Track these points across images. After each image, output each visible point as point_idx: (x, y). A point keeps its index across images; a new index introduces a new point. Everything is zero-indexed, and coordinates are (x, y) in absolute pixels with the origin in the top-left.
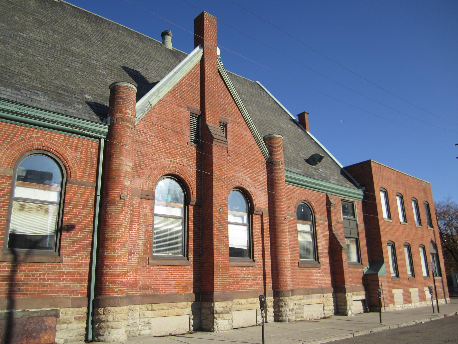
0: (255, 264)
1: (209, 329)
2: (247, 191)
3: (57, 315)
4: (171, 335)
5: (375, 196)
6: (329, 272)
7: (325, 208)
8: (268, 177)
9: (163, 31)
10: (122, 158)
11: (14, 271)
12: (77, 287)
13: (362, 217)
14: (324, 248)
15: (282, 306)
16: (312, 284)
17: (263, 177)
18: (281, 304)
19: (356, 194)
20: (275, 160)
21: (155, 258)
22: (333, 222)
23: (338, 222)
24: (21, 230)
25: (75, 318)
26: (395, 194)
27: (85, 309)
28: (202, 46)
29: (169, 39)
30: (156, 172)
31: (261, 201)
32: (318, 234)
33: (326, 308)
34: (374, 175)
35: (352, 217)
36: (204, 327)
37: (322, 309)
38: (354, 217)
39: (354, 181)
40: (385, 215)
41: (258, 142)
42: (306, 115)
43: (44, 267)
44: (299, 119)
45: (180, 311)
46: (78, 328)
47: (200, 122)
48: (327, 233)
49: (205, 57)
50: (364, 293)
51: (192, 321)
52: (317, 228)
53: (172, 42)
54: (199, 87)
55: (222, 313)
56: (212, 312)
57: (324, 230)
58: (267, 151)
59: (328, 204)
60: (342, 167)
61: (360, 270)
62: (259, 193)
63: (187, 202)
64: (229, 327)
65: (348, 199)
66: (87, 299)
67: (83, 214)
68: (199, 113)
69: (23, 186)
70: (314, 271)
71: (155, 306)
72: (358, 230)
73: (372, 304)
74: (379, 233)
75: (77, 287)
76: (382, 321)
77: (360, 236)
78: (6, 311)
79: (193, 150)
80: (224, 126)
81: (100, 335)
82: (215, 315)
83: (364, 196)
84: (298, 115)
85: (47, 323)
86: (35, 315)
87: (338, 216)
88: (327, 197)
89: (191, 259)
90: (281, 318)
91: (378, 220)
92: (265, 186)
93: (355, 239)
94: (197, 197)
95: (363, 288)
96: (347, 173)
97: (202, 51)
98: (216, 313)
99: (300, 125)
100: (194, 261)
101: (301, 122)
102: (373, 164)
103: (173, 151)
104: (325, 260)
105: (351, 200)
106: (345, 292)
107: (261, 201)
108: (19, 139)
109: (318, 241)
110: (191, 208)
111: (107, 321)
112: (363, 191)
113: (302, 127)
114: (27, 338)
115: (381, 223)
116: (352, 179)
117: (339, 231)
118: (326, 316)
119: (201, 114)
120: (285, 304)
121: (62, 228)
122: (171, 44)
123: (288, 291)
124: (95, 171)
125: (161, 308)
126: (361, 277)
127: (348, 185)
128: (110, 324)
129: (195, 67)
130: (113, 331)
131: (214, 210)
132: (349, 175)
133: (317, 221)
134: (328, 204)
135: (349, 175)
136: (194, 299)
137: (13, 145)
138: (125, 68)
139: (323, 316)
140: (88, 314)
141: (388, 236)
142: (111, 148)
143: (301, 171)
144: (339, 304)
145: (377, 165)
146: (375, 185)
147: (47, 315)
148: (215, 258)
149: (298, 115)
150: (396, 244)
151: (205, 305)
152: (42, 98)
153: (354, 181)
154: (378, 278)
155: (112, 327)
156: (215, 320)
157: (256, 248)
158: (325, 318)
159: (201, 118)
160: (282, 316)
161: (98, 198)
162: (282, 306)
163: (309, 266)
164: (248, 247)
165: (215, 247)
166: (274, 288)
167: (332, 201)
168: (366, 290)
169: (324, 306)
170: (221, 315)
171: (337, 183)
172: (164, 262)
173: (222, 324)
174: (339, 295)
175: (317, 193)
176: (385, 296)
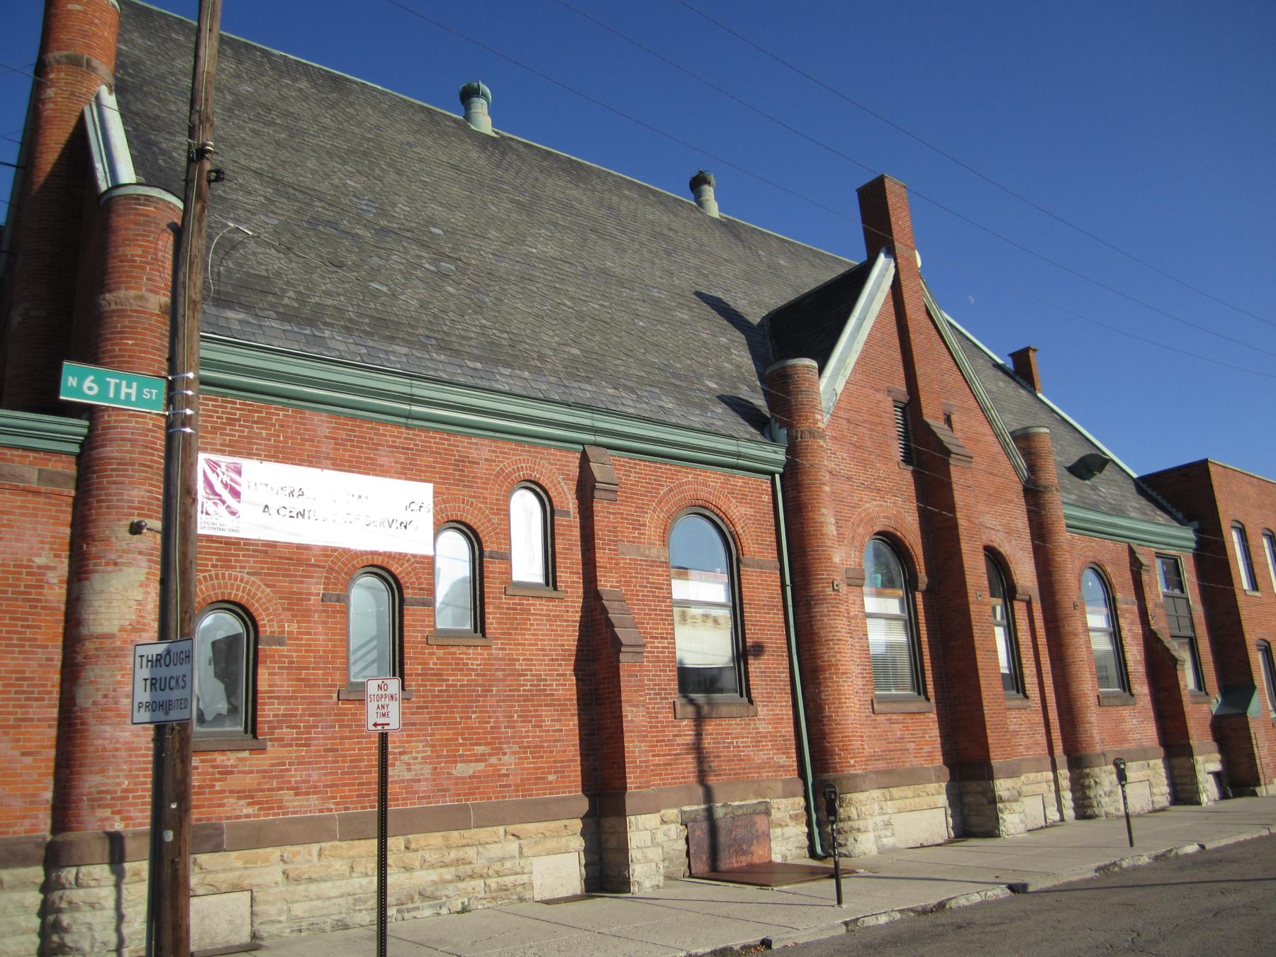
0: (1030, 703)
1: (990, 830)
2: (1000, 553)
3: (767, 813)
4: (922, 846)
5: (1223, 542)
6: (1152, 714)
7: (1128, 575)
8: (1030, 520)
9: (695, 174)
10: (824, 510)
11: (699, 735)
12: (782, 759)
13: (1197, 591)
14: (1136, 662)
15: (1089, 787)
16: (1125, 740)
17: (1021, 522)
18: (1087, 782)
19: (1181, 538)
20: (1042, 482)
21: (882, 700)
22: (1150, 605)
23: (1156, 605)
24: (691, 661)
25: (791, 816)
26: (1260, 531)
27: (801, 801)
28: (891, 252)
29: (709, 192)
30: (861, 530)
31: (1025, 573)
32: (1124, 633)
33: (1155, 790)
34: (1217, 494)
35: (1177, 592)
36: (974, 829)
37: (1147, 791)
38: (1182, 591)
39: (1169, 507)
40: (1245, 584)
41: (1004, 447)
42: (1031, 354)
43: (735, 726)
44: (1015, 364)
45: (925, 800)
46: (797, 835)
47: (908, 417)
48: (1138, 629)
49: (902, 278)
50: (1218, 756)
51: (950, 820)
52: (1121, 621)
53: (490, 114)
54: (896, 342)
55: (1009, 801)
56: (993, 800)
57: (1132, 623)
58: (1022, 464)
59: (1136, 567)
60: (1135, 476)
61: (1205, 707)
62: (1020, 554)
63: (911, 585)
64: (1021, 828)
65: (1167, 552)
66: (801, 782)
67: (769, 624)
68: (905, 398)
69: (679, 578)
70: (1126, 712)
71: (895, 791)
72: (1191, 619)
73: (1239, 779)
74: (1239, 622)
75: (782, 759)
76: (843, 896)
77: (1198, 632)
78: (703, 806)
79: (906, 477)
80: (948, 420)
81: (840, 845)
82: (1000, 805)
83: (1197, 542)
84: (1012, 355)
85: (758, 826)
86: (740, 812)
87: (1157, 587)
88: (1132, 552)
89: (933, 700)
90: (1089, 812)
91: (1234, 595)
92: (1027, 542)
93: (1186, 640)
94: (928, 574)
95: (1214, 746)
96: (1149, 491)
97: (893, 265)
98: (1001, 800)
99: (1018, 378)
100: (937, 703)
101: (1021, 369)
102: (1212, 469)
103: (879, 484)
104: (1141, 688)
105: (1173, 552)
106: (1191, 755)
107: (1025, 573)
108: (666, 489)
109: (1126, 649)
110: (919, 596)
111: (849, 818)
112: (1196, 531)
113: (1024, 383)
114: (736, 852)
115: (1241, 599)
116: (1164, 503)
117: (1160, 625)
118: (1157, 807)
119: (910, 401)
120: (1096, 783)
121: (744, 652)
122: (489, 120)
123: (1098, 755)
124: (773, 538)
125: (903, 794)
126: (1208, 723)
127: (1161, 520)
128: (856, 824)
129: (886, 302)
130: (861, 837)
131: (971, 599)
132: (1154, 494)
133: (1119, 605)
134: (1136, 567)
135: (1154, 494)
136: (948, 778)
137: (660, 502)
138: (699, 294)
139: (1150, 807)
140: (807, 809)
141: (1258, 630)
142: (799, 492)
143: (1073, 497)
144: (1179, 781)
145: (1220, 469)
146: (1221, 515)
147: (754, 813)
148: (984, 695)
149: (1012, 355)
150: (1273, 646)
151: (973, 786)
152: (668, 403)
153: (1169, 507)
154: (1247, 723)
155: (859, 830)
156: (1000, 815)
157: (1026, 671)
158: (1155, 811)
159: (911, 410)
160: (1091, 806)
161: (789, 590)
162: (1089, 787)
163: (1117, 702)
164: (1009, 668)
165: (981, 673)
166: (1067, 751)
167: (1143, 559)
168: (1222, 750)
169: (1151, 786)
170: (1007, 805)
171: (1142, 517)
172: (895, 707)
173: (1012, 821)
174: (1177, 762)
175: (1110, 544)
176: (1264, 761)
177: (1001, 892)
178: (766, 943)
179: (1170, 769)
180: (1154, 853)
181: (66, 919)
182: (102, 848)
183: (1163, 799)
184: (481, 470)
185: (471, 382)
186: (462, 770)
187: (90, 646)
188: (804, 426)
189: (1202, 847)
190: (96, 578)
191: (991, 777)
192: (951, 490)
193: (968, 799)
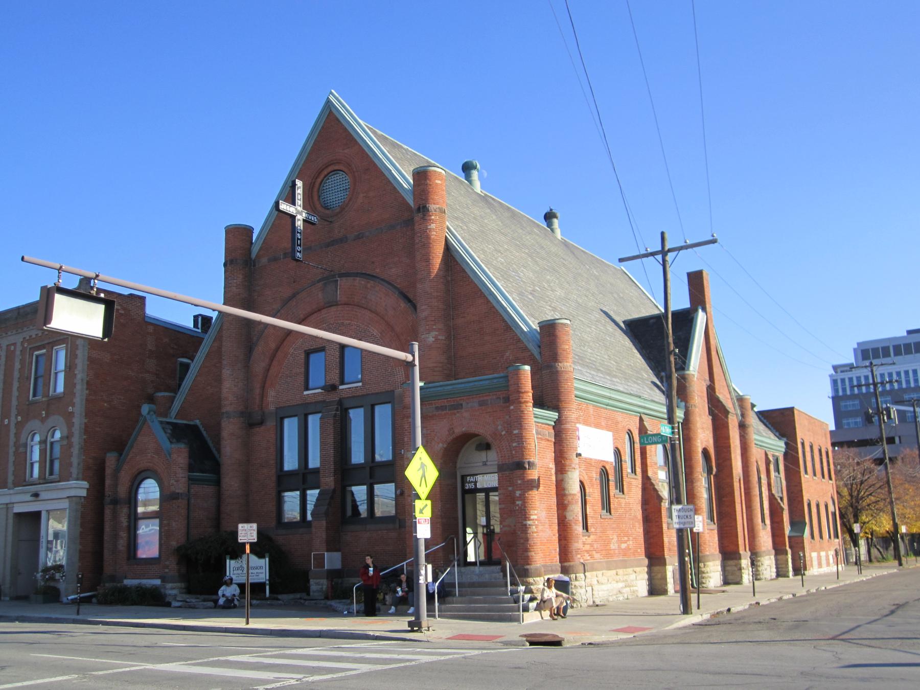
19: (777, 446)
28: (704, 309)
29: (475, 174)
102: (796, 412)
112: (786, 444)
151: (731, 562)
173: (813, 571)
174: (779, 557)
177: (791, 596)
178: (758, 603)
179: (650, 573)
180: (712, 612)
181: (574, 591)
182: (581, 568)
183: (774, 575)
184: (620, 426)
185: (612, 387)
186: (624, 546)
187: (570, 498)
188: (692, 402)
189: (794, 595)
190: (569, 473)
191: (740, 558)
192: (728, 429)
193: (728, 568)
